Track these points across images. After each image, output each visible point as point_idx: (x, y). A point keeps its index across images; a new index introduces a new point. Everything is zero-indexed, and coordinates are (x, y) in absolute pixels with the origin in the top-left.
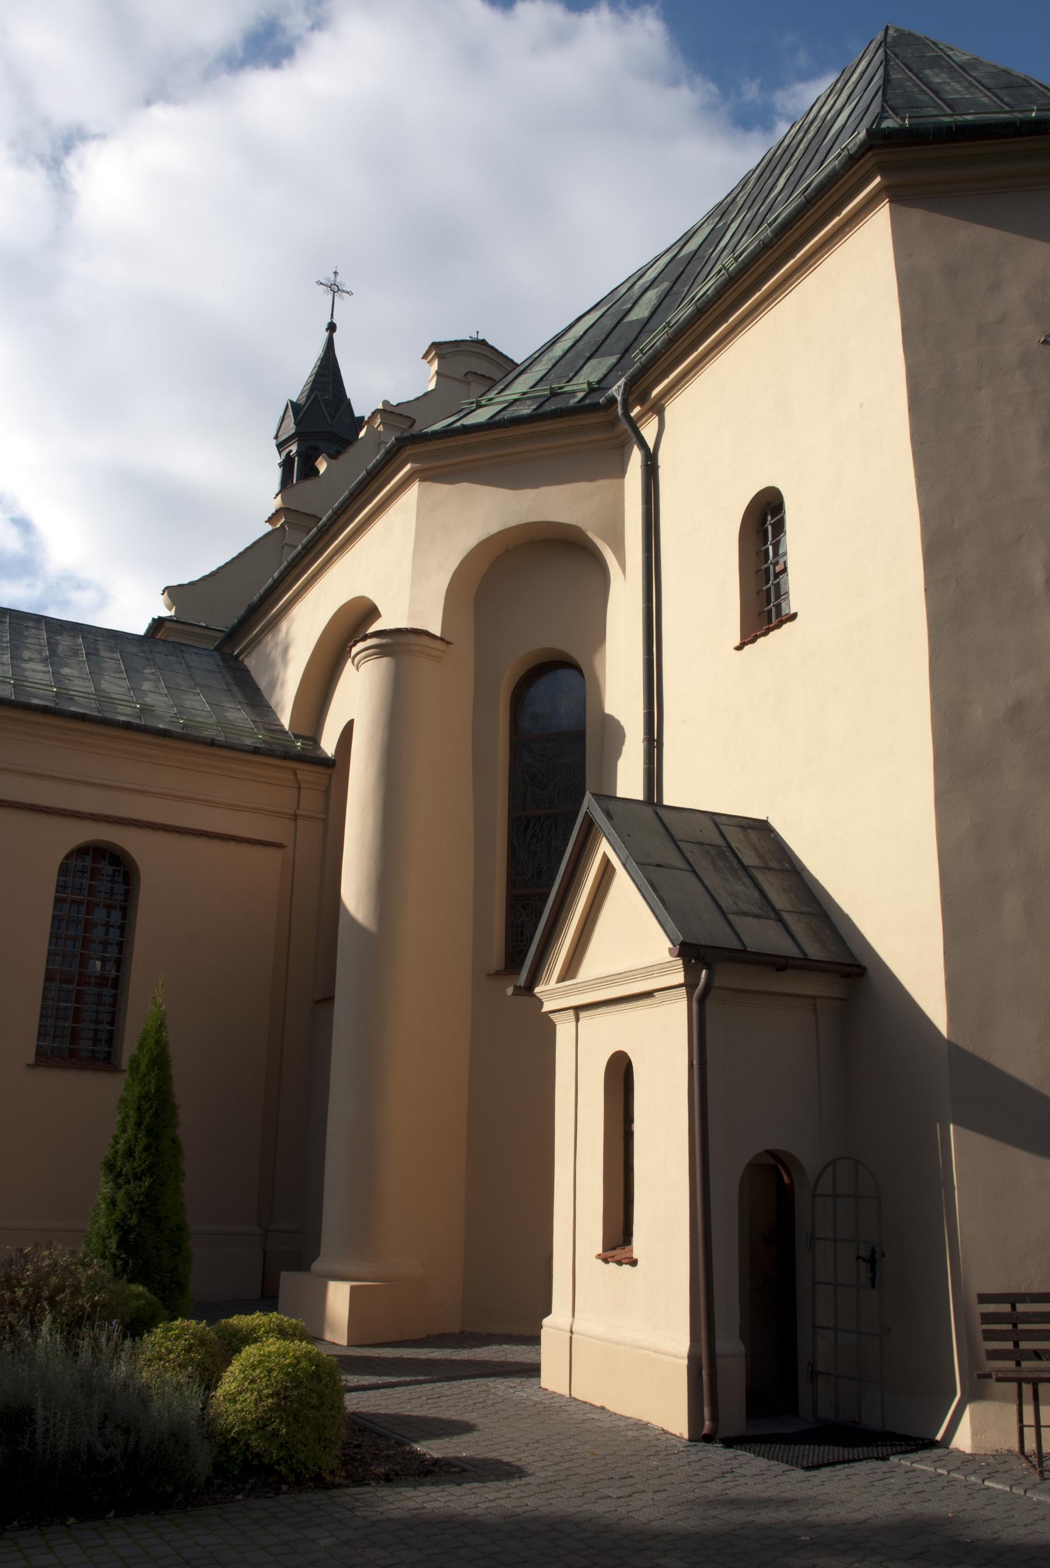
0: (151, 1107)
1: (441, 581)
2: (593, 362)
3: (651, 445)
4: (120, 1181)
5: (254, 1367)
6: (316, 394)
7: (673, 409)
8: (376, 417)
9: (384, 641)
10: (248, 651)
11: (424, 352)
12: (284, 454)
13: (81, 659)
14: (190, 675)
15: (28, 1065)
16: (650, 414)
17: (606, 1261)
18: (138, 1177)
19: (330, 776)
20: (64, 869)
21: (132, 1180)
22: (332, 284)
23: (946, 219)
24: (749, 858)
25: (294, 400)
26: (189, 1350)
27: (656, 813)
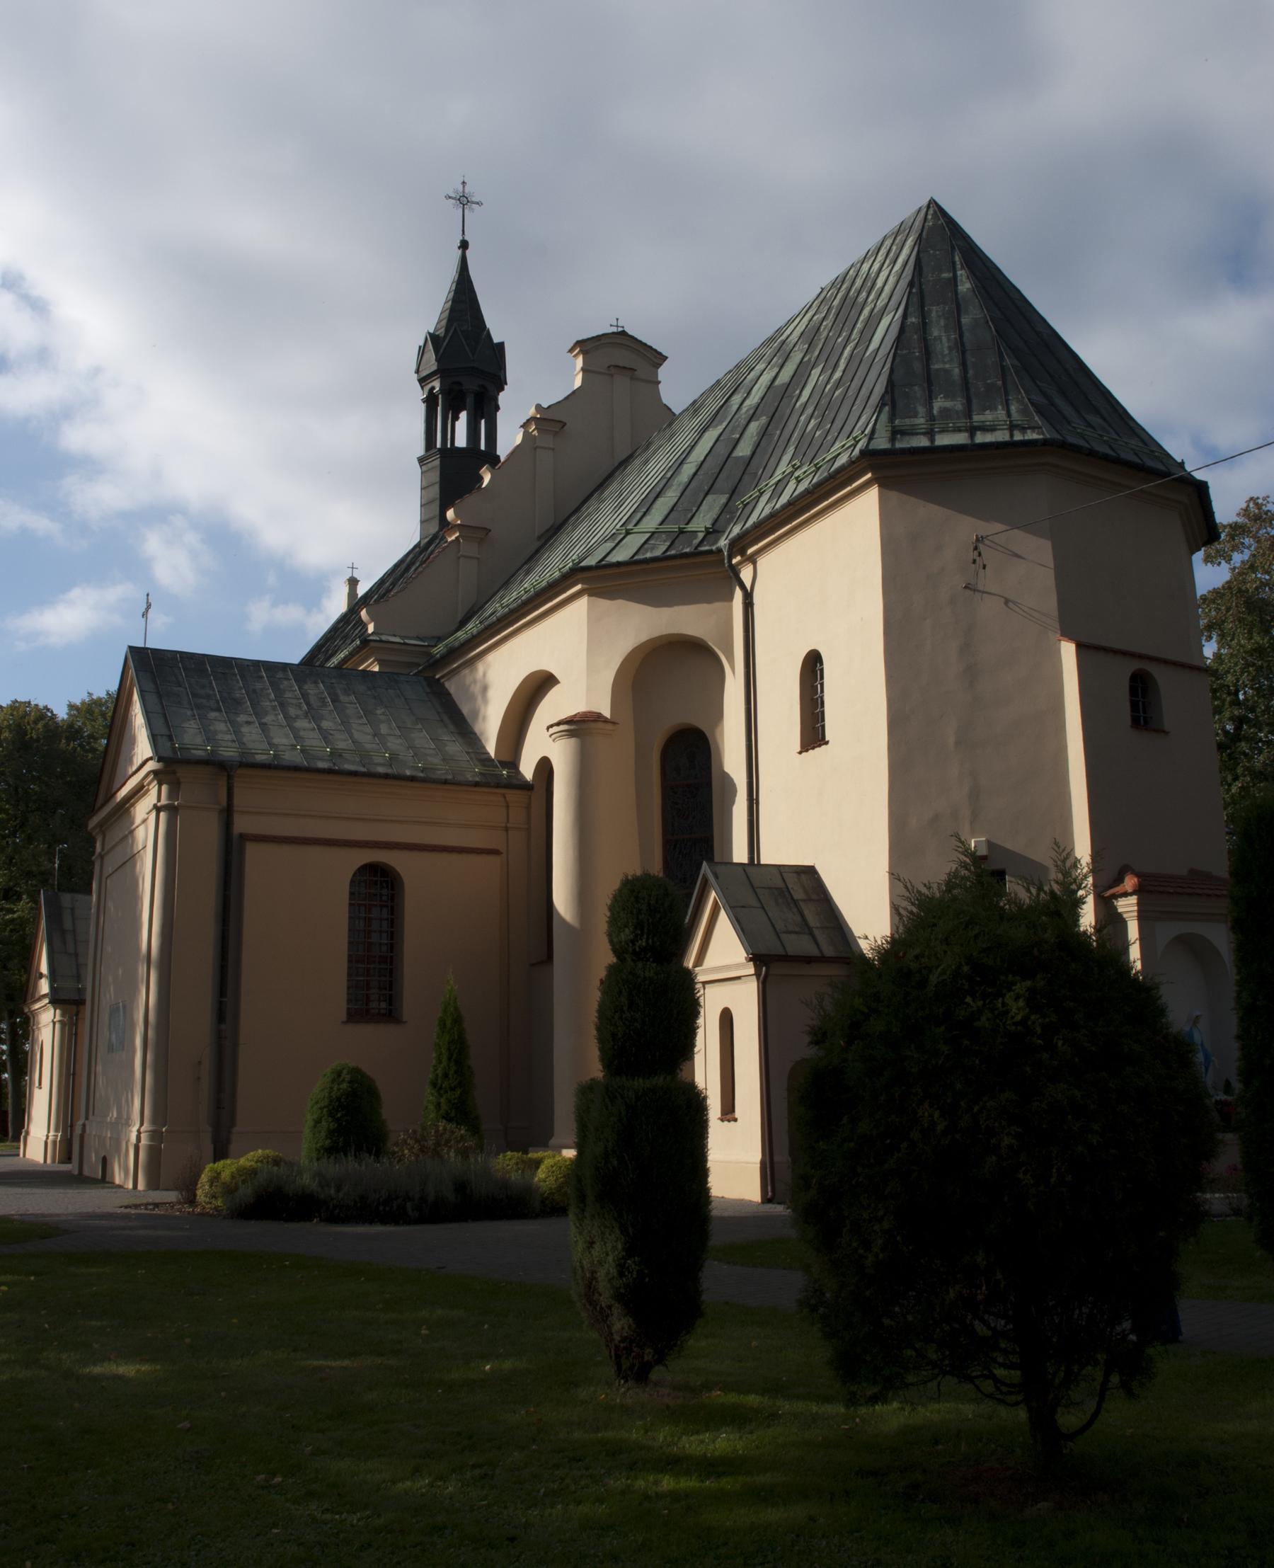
0: (456, 1048)
1: (608, 676)
2: (710, 498)
3: (748, 586)
4: (442, 1092)
5: (552, 1167)
6: (455, 329)
7: (762, 562)
8: (531, 424)
9: (572, 727)
10: (449, 676)
11: (570, 347)
12: (427, 388)
13: (330, 709)
14: (410, 709)
15: (343, 1022)
16: (747, 562)
17: (722, 1120)
18: (453, 1089)
19: (530, 796)
20: (352, 881)
21: (449, 1092)
22: (461, 197)
23: (913, 500)
24: (798, 894)
25: (432, 331)
26: (517, 1164)
27: (744, 870)
